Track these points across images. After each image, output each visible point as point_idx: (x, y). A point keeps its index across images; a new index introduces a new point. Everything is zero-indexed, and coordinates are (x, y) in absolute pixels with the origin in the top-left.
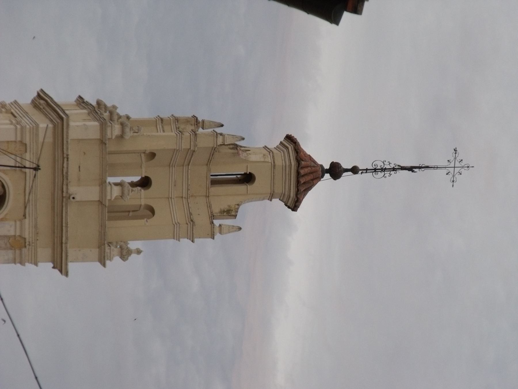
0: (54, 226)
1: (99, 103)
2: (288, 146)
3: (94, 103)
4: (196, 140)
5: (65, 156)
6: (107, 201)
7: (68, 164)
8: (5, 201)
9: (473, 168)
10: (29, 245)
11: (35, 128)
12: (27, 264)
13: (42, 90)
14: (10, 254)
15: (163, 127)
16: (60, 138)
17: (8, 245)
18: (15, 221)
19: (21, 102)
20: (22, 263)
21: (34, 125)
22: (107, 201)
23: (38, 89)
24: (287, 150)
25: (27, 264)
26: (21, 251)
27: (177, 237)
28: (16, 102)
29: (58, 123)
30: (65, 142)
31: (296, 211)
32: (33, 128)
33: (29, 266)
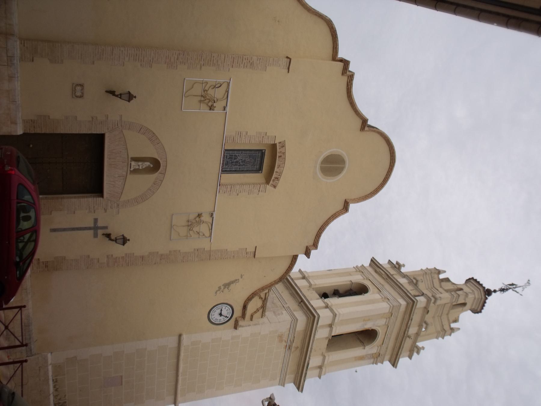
1: (397, 263)
3: (395, 263)
5: (411, 318)
6: (50, 368)
7: (411, 322)
9: (521, 296)
10: (381, 355)
11: (399, 306)
12: (277, 405)
13: (373, 258)
14: (372, 360)
17: (372, 357)
20: (376, 364)
21: (399, 304)
22: (50, 368)
23: (372, 257)
25: (277, 405)
27: (437, 338)
30: (412, 312)
31: (368, 120)
32: (398, 306)
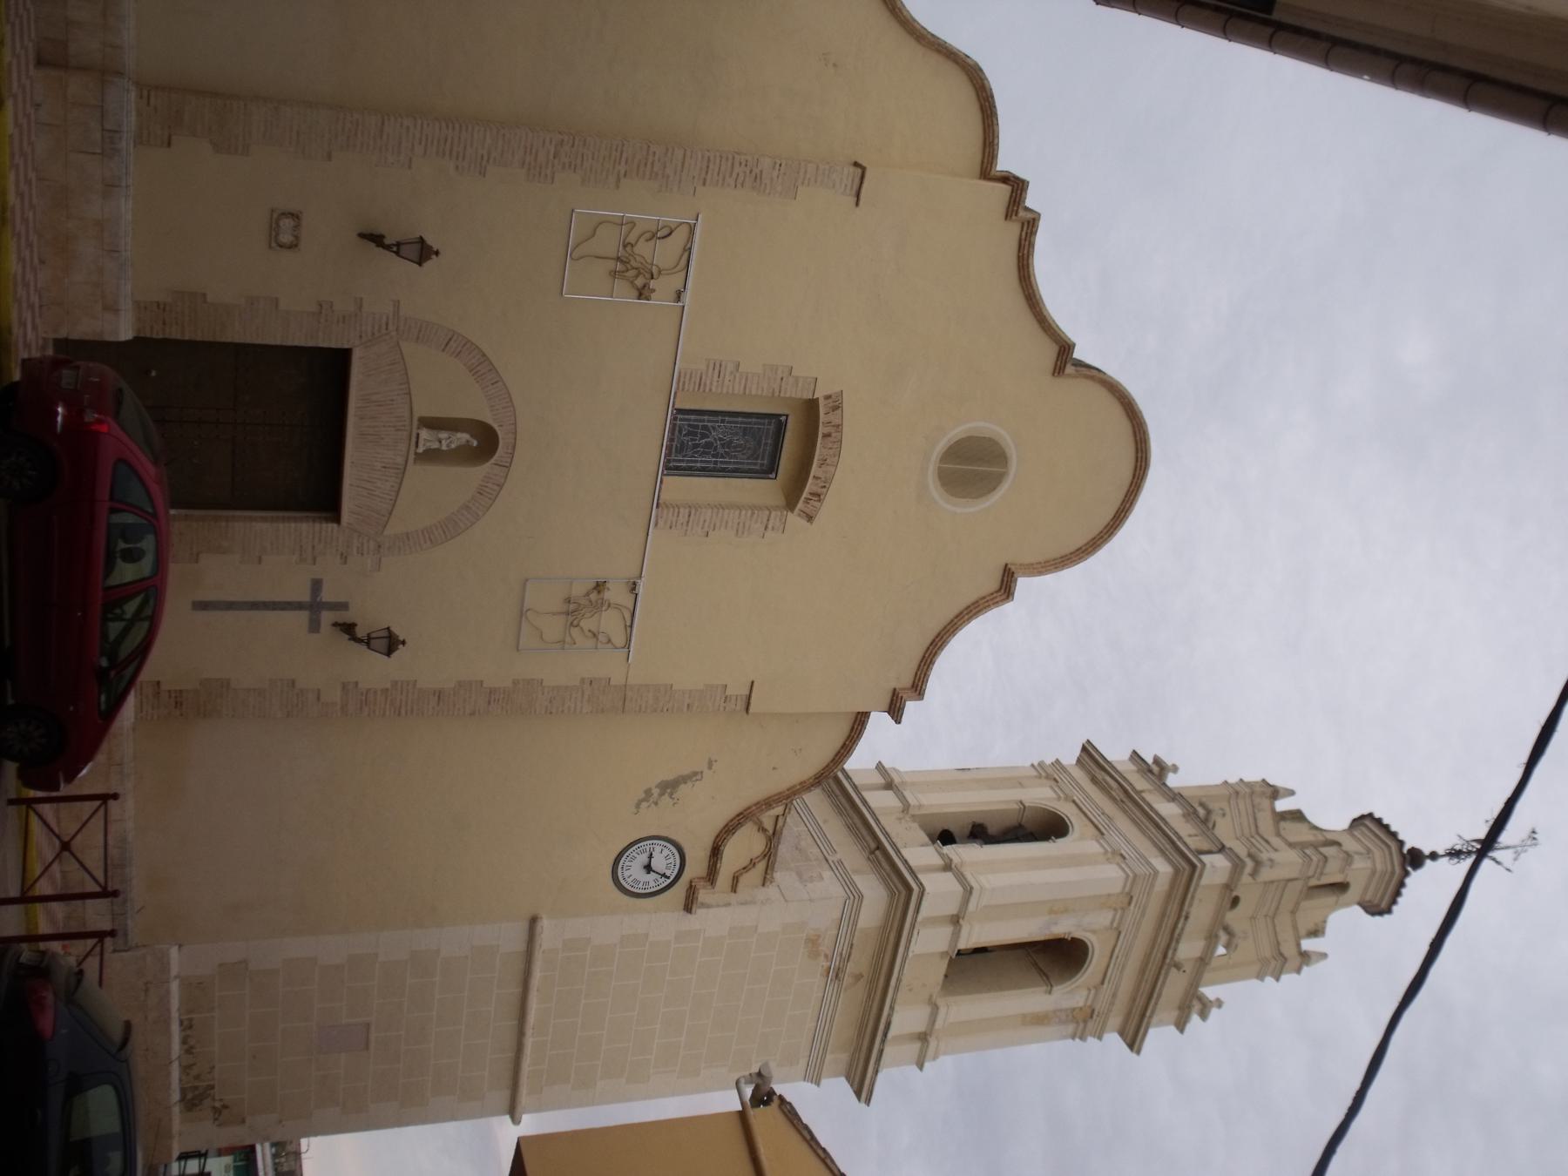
0: (1138, 991)
2: (1390, 843)
3: (1150, 760)
4: (1324, 866)
5: (1184, 913)
8: (1082, 966)
13: (1088, 741)
14: (1071, 1028)
15: (1237, 803)
16: (1181, 890)
18: (1089, 990)
19: (1064, 762)
20: (1083, 1038)
23: (1084, 741)
24: (1387, 853)
26: (403, 244)
27: (1260, 976)
28: (1057, 761)
29: (1184, 869)
33: (1091, 1040)
